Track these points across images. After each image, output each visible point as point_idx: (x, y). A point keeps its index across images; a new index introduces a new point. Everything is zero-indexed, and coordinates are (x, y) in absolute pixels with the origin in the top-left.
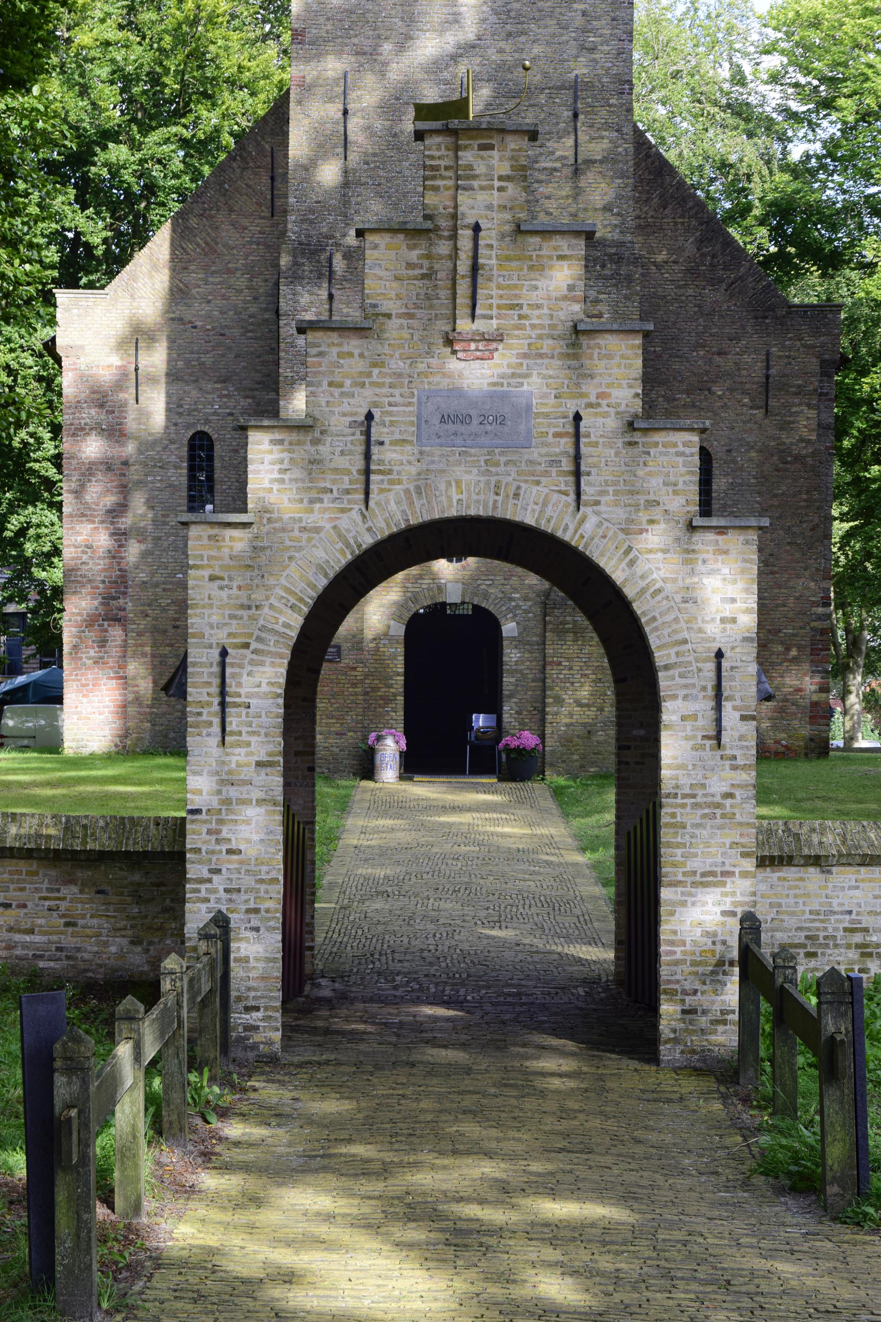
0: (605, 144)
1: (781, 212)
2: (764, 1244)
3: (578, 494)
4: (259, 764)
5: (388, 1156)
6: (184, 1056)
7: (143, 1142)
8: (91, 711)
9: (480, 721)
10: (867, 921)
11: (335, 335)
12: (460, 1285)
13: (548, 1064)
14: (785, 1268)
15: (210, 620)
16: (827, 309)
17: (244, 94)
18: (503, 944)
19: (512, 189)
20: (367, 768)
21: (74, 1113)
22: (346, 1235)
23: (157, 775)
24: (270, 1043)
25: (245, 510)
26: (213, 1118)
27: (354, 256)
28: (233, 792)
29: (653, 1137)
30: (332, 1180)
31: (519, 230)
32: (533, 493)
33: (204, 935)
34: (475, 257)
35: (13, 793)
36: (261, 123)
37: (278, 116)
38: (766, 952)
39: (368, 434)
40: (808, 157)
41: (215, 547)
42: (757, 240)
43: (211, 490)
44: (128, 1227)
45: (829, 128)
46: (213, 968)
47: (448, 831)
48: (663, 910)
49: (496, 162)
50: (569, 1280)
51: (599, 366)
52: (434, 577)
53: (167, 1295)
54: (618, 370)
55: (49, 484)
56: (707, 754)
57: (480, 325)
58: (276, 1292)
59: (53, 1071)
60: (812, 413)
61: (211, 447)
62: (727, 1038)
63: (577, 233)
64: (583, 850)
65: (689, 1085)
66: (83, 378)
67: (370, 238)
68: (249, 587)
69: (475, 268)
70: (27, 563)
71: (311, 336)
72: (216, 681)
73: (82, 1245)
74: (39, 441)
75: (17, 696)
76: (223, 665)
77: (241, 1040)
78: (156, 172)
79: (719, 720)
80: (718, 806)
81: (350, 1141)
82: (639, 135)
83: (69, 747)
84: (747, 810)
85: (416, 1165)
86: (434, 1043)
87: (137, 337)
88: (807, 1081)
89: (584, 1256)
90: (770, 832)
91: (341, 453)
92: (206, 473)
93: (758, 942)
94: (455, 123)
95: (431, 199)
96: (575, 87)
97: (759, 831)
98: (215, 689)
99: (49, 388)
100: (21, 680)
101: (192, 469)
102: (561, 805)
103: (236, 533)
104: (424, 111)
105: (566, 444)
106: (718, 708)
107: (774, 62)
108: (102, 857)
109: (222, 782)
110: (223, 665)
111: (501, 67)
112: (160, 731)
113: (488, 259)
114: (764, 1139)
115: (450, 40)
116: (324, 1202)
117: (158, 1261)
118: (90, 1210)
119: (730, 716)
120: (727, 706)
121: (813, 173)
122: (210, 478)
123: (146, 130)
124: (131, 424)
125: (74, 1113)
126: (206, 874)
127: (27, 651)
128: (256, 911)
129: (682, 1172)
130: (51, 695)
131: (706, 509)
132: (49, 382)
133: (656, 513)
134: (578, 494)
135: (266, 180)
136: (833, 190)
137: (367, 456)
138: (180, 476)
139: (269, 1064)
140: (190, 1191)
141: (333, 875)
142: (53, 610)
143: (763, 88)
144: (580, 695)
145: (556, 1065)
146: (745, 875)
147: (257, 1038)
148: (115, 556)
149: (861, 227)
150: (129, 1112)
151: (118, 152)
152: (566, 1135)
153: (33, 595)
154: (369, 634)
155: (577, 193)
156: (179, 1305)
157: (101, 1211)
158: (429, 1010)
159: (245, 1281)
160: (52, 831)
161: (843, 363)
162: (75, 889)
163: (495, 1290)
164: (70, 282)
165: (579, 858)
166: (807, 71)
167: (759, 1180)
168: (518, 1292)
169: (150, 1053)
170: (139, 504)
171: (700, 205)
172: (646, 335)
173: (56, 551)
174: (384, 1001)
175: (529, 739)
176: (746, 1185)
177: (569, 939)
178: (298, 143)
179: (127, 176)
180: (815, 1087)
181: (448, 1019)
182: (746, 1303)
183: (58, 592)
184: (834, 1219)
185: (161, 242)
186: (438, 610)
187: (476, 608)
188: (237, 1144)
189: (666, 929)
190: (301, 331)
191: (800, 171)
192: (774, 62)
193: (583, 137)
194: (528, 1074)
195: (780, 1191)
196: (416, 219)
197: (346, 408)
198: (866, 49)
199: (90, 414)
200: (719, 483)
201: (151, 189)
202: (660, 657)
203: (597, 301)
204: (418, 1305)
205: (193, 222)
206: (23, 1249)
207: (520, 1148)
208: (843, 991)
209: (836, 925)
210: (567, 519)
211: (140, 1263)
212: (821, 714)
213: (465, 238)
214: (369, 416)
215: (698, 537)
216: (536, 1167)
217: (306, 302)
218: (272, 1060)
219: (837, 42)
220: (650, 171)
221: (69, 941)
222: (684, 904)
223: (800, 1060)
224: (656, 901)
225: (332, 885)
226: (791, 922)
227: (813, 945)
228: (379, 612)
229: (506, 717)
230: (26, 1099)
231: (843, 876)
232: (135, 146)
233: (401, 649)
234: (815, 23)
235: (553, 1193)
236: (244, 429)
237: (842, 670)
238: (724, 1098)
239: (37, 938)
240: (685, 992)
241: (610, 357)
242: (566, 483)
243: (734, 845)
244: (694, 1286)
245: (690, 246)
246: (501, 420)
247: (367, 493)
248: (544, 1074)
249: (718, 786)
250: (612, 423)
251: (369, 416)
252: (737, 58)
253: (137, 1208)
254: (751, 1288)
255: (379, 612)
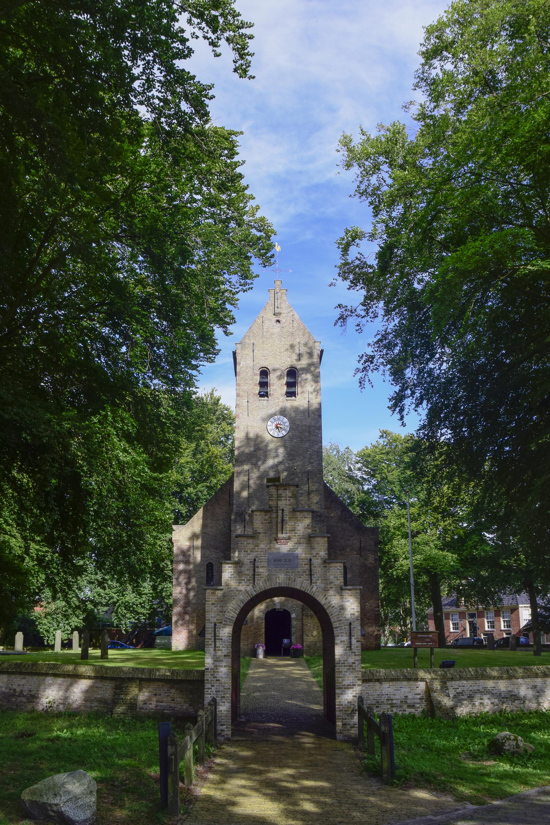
0: (316, 487)
1: (362, 503)
2: (367, 792)
3: (311, 580)
4: (225, 656)
5: (261, 768)
6: (204, 739)
7: (192, 764)
8: (179, 640)
9: (286, 641)
10: (392, 697)
11: (245, 539)
12: (282, 806)
13: (305, 740)
14: (372, 799)
15: (212, 615)
16: (376, 528)
17: (223, 475)
18: (293, 705)
19: (292, 500)
20: (254, 654)
21: (173, 757)
22: (249, 792)
23: (197, 656)
24: (228, 735)
25: (221, 585)
26: (212, 757)
27: (251, 516)
28: (218, 664)
29: (335, 761)
30: (245, 776)
31: (294, 511)
32: (299, 580)
33: (210, 704)
34: (283, 517)
35: (158, 662)
36: (227, 482)
37: (231, 481)
38: (365, 707)
39: (254, 564)
40: (368, 489)
41: (212, 597)
42: (357, 511)
43: (213, 578)
44: (189, 789)
45: (374, 482)
46: (212, 714)
47: (277, 673)
48: (336, 695)
49: (288, 493)
50: (312, 804)
51: (316, 546)
52: (273, 601)
53: (199, 809)
54: (321, 548)
55: (170, 577)
56: (348, 652)
57: (284, 535)
58: (230, 808)
59: (167, 745)
60: (373, 556)
61: (212, 566)
62: (354, 732)
63: (309, 511)
64: (314, 677)
65: (345, 746)
66: (179, 548)
67: (255, 513)
68: (222, 607)
69: (283, 520)
70: (164, 598)
71: (239, 539)
72: (213, 633)
73: (175, 795)
74: (167, 565)
75: (160, 634)
76: (215, 628)
77: (220, 734)
78: (200, 494)
79: (351, 642)
80: (351, 666)
81: (250, 764)
82: (325, 484)
83: (174, 649)
84: (359, 667)
85: (268, 771)
86: (274, 734)
87: (194, 536)
88: (377, 744)
89: (316, 797)
90: (365, 673)
91: (247, 570)
92: (210, 575)
93: (363, 704)
94: (277, 483)
95: (271, 503)
96: (308, 472)
97: (362, 672)
98: (213, 635)
99: (170, 551)
100: (161, 629)
101: (207, 572)
102: (308, 664)
103: (219, 592)
104: (269, 480)
105: (307, 567)
106: (350, 639)
107: (359, 465)
108: (182, 681)
109: (214, 661)
110: (215, 628)
111: (289, 467)
112: (198, 644)
113: (286, 518)
114: (366, 761)
115: (276, 460)
116: (243, 782)
117: (197, 799)
118: (177, 784)
119: (354, 641)
120: (353, 638)
121: (370, 493)
122: (212, 575)
123: (197, 484)
124: (191, 560)
125: (173, 757)
126: (210, 687)
127: (163, 622)
128: (224, 697)
129: (343, 771)
130: (169, 633)
131: (346, 584)
132: (170, 549)
133: (332, 585)
134: (311, 580)
135: (228, 496)
136: (376, 497)
137: (254, 571)
138: (204, 574)
139: (229, 741)
140: (205, 779)
141: (245, 685)
142: (170, 610)
143: (356, 472)
144: (314, 635)
145: (307, 740)
146: (359, 685)
147: (224, 733)
148: (187, 596)
149: (383, 507)
150: (189, 754)
151: (191, 490)
152: (311, 761)
153: (165, 606)
154: (255, 617)
155: (309, 499)
156: (202, 812)
157: (181, 784)
158: (272, 725)
159: (221, 805)
160: (168, 674)
161: (380, 542)
162: (174, 690)
163: (291, 807)
164: (176, 523)
165: (313, 680)
166: (367, 468)
167: (364, 773)
168: (297, 808)
169: (194, 738)
170: (194, 582)
171: (342, 502)
172: (328, 537)
173: (171, 595)
174: (260, 722)
175: (299, 646)
176: (361, 775)
177: (311, 703)
178: (237, 486)
179: (193, 495)
180: (379, 745)
181: (277, 727)
182: (362, 810)
183: (171, 606)
184: (386, 784)
185: (200, 513)
186: (274, 610)
187: (284, 610)
188: (218, 764)
189: (337, 701)
190: (237, 537)
191: (367, 493)
192: (359, 465)
193: (310, 485)
194: (300, 743)
195: (370, 776)
196: (267, 508)
197: (248, 557)
198: (382, 462)
199: (181, 558)
200: (349, 576)
201: (198, 498)
202: (335, 625)
203: (315, 527)
204: (269, 812)
205: (209, 507)
206: (159, 795)
207: (298, 765)
208: (387, 719)
209: (384, 698)
210: (308, 587)
211: (191, 800)
212: (378, 637)
213: (280, 513)
214: (255, 560)
215: (344, 592)
216: (302, 771)
217: (239, 529)
218: (228, 739)
219: (375, 461)
220: (328, 494)
221: (173, 705)
222: (342, 694)
223: (375, 737)
224: (334, 693)
225: (245, 688)
226: (371, 698)
227: (378, 704)
228: (259, 611)
229: (293, 640)
230: (160, 751)
231: (386, 685)
232: (195, 488)
233: (264, 621)
234: (369, 456)
235: (307, 779)
236: (221, 563)
237: (383, 625)
238: (354, 749)
239: (164, 704)
240: (343, 719)
241: (319, 543)
242: (307, 577)
243: (355, 677)
244: (347, 805)
245: (339, 513)
246: (290, 560)
247: (254, 580)
248: (304, 743)
249: (351, 660)
250: (319, 561)
251: (255, 560)
252: (350, 465)
253: (191, 783)
254: (363, 805)
255: (259, 611)
